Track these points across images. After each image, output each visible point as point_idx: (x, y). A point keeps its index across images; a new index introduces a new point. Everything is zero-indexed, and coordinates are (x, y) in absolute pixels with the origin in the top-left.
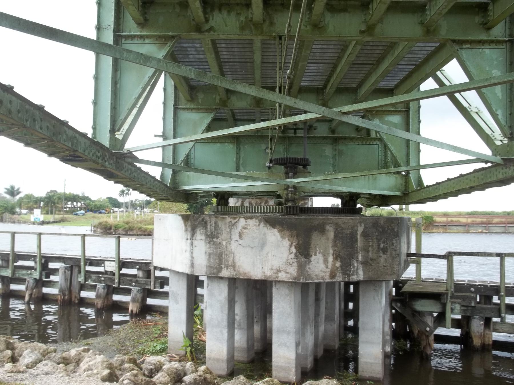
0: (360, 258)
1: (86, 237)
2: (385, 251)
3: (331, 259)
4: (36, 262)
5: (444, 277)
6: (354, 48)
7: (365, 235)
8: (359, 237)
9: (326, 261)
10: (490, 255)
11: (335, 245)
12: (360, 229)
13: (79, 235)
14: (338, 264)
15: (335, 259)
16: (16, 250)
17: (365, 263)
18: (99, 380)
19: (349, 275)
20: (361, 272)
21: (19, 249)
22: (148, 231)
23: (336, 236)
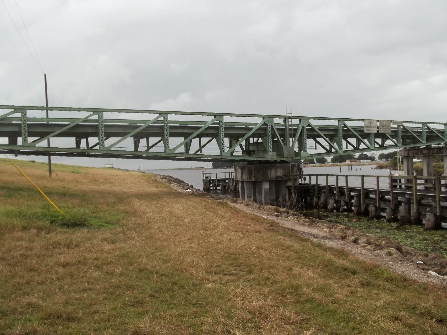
0: (253, 175)
1: (348, 177)
2: (259, 173)
3: (247, 176)
4: (376, 195)
5: (335, 185)
6: (125, 171)
7: (254, 169)
8: (253, 170)
9: (246, 176)
10: (323, 175)
11: (248, 172)
12: (253, 168)
13: (325, 175)
14: (249, 177)
15: (248, 175)
16: (365, 187)
17: (254, 176)
18: (403, 320)
19: (251, 179)
20: (253, 179)
21: (350, 185)
22: (440, 172)
23: (248, 170)
